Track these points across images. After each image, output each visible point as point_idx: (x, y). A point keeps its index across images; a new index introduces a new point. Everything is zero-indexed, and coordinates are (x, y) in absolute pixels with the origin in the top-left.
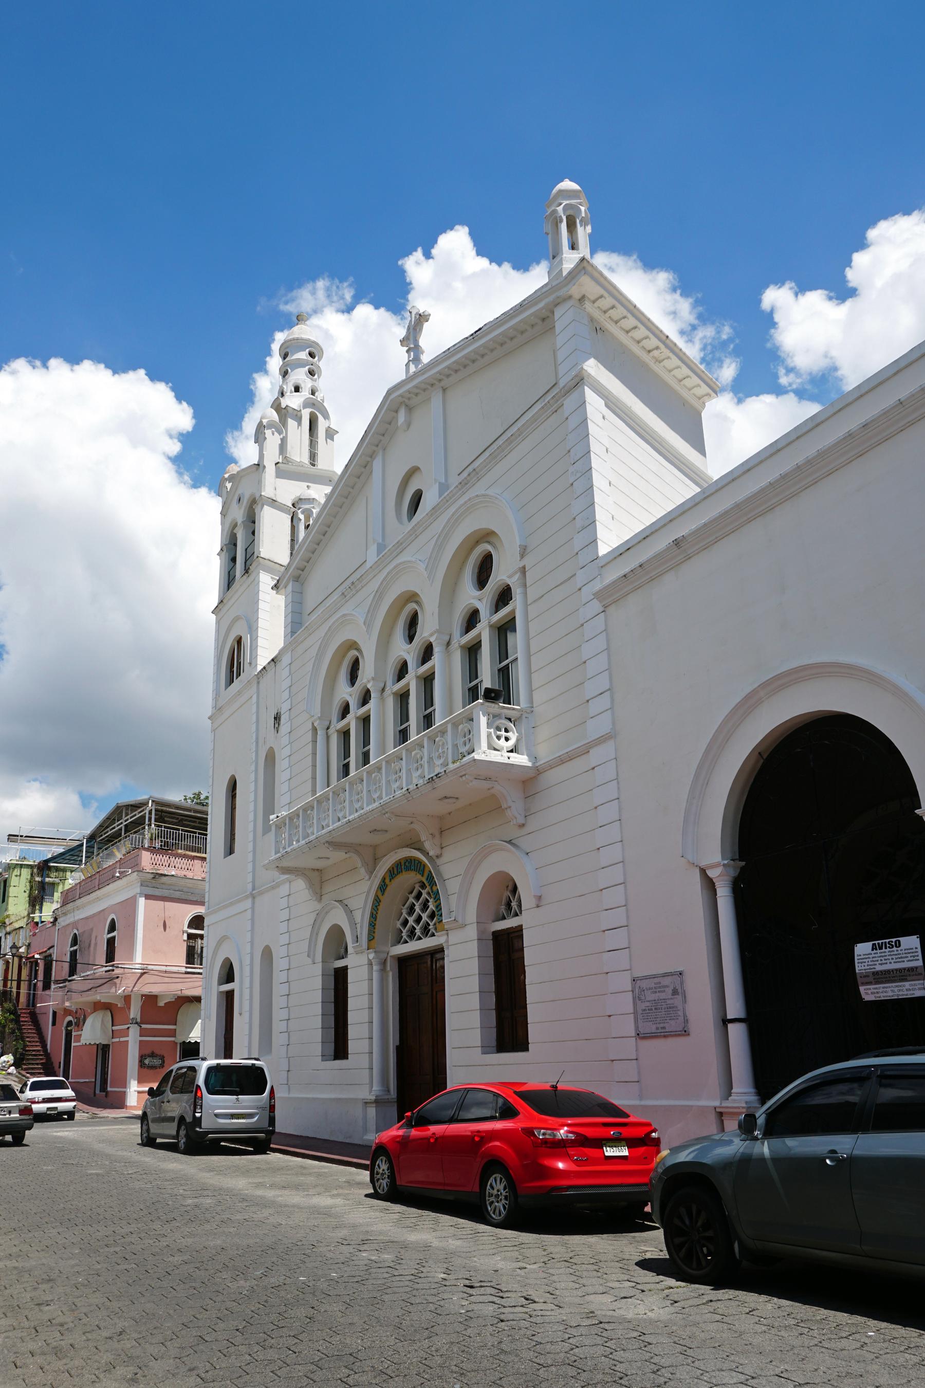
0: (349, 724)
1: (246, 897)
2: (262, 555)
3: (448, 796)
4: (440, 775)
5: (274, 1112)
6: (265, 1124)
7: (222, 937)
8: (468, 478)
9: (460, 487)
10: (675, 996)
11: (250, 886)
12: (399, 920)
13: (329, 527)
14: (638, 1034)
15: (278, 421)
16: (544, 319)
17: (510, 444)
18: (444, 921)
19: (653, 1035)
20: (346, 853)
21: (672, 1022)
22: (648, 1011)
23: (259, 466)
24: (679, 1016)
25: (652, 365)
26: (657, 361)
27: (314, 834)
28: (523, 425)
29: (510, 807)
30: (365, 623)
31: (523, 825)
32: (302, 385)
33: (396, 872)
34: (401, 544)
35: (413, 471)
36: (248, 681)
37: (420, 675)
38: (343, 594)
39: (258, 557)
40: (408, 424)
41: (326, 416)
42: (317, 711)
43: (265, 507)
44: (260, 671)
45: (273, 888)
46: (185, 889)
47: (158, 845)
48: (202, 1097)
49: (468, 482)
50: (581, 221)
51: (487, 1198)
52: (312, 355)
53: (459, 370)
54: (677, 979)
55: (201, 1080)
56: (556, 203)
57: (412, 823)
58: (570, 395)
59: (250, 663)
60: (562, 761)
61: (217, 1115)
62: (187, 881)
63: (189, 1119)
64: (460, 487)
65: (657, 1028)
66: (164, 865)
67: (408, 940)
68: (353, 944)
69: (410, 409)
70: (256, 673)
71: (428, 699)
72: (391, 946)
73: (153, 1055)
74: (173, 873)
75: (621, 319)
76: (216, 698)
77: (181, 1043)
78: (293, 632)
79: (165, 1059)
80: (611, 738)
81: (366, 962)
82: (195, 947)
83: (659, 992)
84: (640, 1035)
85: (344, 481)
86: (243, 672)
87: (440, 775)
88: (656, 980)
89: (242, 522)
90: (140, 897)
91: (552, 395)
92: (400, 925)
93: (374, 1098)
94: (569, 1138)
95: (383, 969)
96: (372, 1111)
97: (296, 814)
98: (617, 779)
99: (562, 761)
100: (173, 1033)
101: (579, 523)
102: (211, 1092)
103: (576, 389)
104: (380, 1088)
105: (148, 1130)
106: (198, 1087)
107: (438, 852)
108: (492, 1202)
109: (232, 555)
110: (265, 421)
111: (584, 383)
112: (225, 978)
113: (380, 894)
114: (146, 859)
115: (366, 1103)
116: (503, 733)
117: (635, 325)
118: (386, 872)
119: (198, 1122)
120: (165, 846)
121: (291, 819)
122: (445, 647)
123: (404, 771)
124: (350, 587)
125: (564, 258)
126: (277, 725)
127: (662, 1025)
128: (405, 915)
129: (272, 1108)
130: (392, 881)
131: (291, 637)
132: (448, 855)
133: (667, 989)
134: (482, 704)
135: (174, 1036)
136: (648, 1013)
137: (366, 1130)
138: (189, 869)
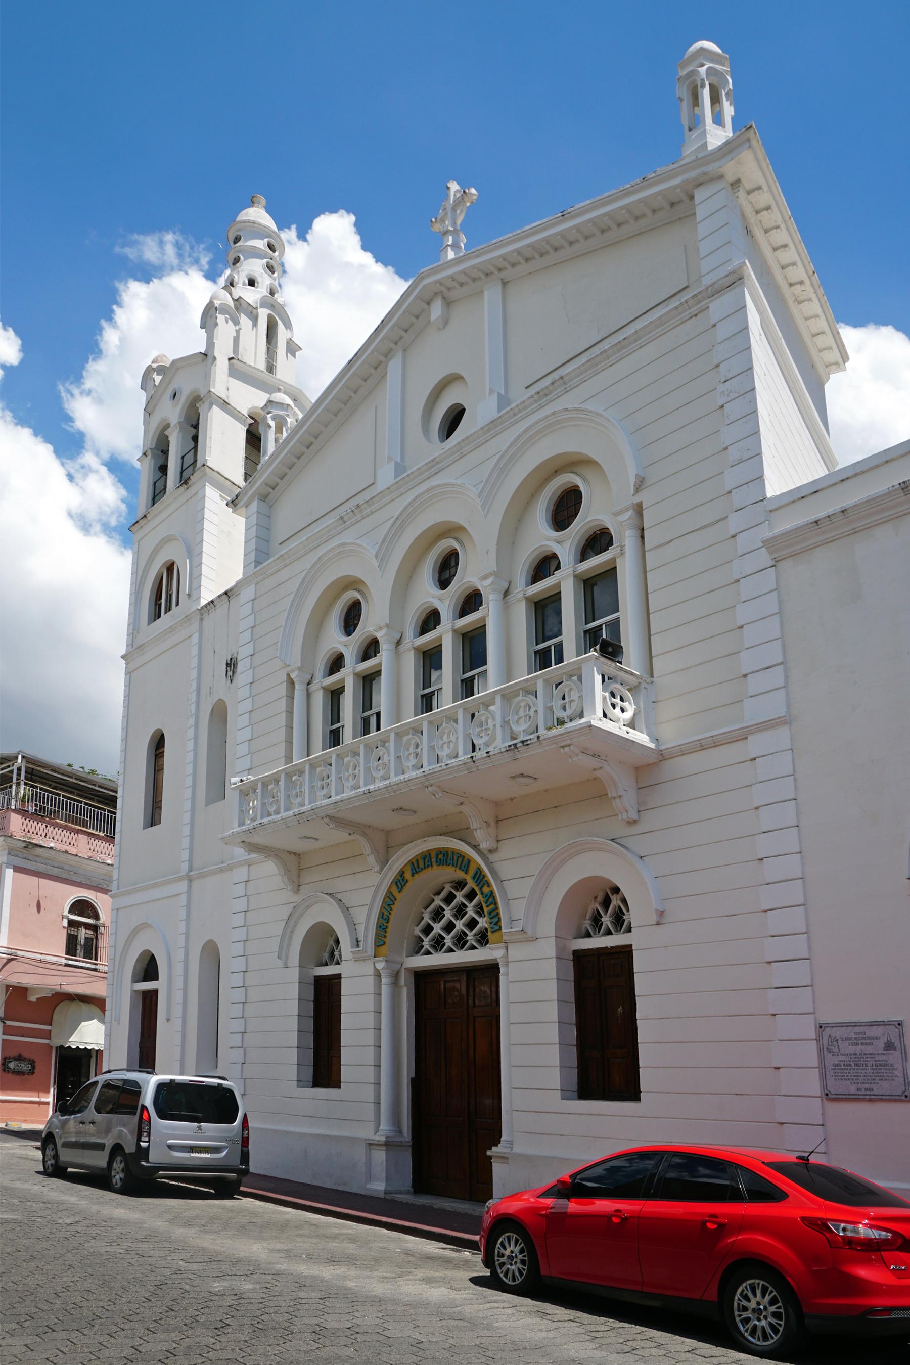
0: (343, 680)
1: (181, 879)
2: (209, 464)
3: (526, 774)
4: (529, 742)
5: (247, 1146)
6: (236, 1161)
7: (141, 924)
8: (551, 388)
9: (536, 397)
10: (890, 1052)
11: (185, 867)
12: (417, 925)
13: (316, 438)
14: (827, 1095)
15: (233, 307)
16: (673, 203)
17: (619, 351)
18: (504, 930)
19: (851, 1097)
20: (350, 834)
21: (886, 1085)
22: (843, 1067)
23: (206, 357)
24: (897, 1076)
25: (791, 302)
26: (796, 300)
27: (278, 814)
28: (643, 328)
29: (620, 797)
30: (376, 556)
31: (635, 822)
32: (259, 279)
33: (421, 865)
34: (438, 463)
35: (453, 379)
36: (187, 616)
37: (358, 672)
38: (342, 518)
39: (204, 465)
40: (446, 322)
41: (288, 325)
42: (295, 660)
43: (215, 407)
44: (206, 606)
45: (222, 870)
46: (66, 867)
47: (31, 809)
48: (150, 1122)
49: (551, 393)
50: (727, 94)
51: (496, 1258)
52: (271, 247)
53: (533, 258)
54: (894, 1032)
55: (148, 1098)
56: (696, 63)
57: (462, 804)
58: (721, 296)
59: (189, 595)
60: (701, 746)
61: (170, 1147)
62: (69, 857)
63: (130, 1148)
64: (536, 397)
65: (858, 1089)
66: (39, 834)
67: (432, 951)
68: (352, 948)
69: (448, 303)
70: (199, 608)
71: (367, 700)
72: (407, 957)
73: (19, 1058)
74: (52, 845)
75: (772, 228)
76: (133, 633)
77: (57, 1048)
78: (258, 563)
79: (35, 1064)
80: (785, 724)
81: (372, 971)
82: (77, 936)
83: (862, 1044)
84: (830, 1096)
85: (344, 381)
86: (177, 604)
87: (529, 742)
88: (857, 1029)
89: (179, 423)
90: (7, 867)
91: (694, 293)
92: (334, 941)
93: (383, 1139)
94: (883, 1237)
95: (395, 983)
96: (380, 1156)
97: (253, 787)
98: (794, 775)
99: (702, 746)
100: (47, 1035)
101: (734, 454)
102: (162, 1115)
103: (730, 290)
104: (392, 1128)
105: (56, 1157)
106: (144, 1108)
107: (494, 845)
108: (503, 1264)
109: (160, 463)
110: (217, 303)
111: (743, 283)
112: (142, 974)
113: (395, 890)
114: (16, 823)
115: (370, 1144)
116: (617, 701)
117: (785, 243)
118: (407, 864)
119: (144, 1153)
120: (40, 812)
121: (265, 785)
122: (502, 596)
123: (333, 778)
124: (352, 511)
125: (708, 131)
126: (230, 673)
127: (867, 1086)
128: (427, 919)
129: (245, 1141)
130: (416, 876)
131: (255, 567)
132: (507, 850)
133: (875, 1042)
134: (597, 658)
135: (49, 1038)
136: (843, 1069)
137: (370, 1177)
138: (72, 843)
